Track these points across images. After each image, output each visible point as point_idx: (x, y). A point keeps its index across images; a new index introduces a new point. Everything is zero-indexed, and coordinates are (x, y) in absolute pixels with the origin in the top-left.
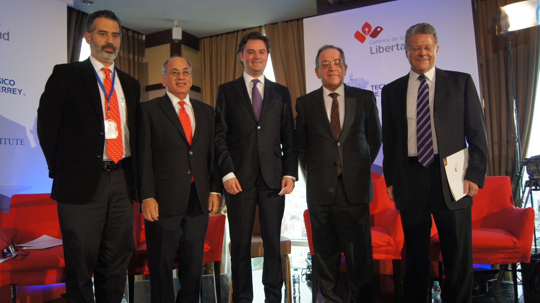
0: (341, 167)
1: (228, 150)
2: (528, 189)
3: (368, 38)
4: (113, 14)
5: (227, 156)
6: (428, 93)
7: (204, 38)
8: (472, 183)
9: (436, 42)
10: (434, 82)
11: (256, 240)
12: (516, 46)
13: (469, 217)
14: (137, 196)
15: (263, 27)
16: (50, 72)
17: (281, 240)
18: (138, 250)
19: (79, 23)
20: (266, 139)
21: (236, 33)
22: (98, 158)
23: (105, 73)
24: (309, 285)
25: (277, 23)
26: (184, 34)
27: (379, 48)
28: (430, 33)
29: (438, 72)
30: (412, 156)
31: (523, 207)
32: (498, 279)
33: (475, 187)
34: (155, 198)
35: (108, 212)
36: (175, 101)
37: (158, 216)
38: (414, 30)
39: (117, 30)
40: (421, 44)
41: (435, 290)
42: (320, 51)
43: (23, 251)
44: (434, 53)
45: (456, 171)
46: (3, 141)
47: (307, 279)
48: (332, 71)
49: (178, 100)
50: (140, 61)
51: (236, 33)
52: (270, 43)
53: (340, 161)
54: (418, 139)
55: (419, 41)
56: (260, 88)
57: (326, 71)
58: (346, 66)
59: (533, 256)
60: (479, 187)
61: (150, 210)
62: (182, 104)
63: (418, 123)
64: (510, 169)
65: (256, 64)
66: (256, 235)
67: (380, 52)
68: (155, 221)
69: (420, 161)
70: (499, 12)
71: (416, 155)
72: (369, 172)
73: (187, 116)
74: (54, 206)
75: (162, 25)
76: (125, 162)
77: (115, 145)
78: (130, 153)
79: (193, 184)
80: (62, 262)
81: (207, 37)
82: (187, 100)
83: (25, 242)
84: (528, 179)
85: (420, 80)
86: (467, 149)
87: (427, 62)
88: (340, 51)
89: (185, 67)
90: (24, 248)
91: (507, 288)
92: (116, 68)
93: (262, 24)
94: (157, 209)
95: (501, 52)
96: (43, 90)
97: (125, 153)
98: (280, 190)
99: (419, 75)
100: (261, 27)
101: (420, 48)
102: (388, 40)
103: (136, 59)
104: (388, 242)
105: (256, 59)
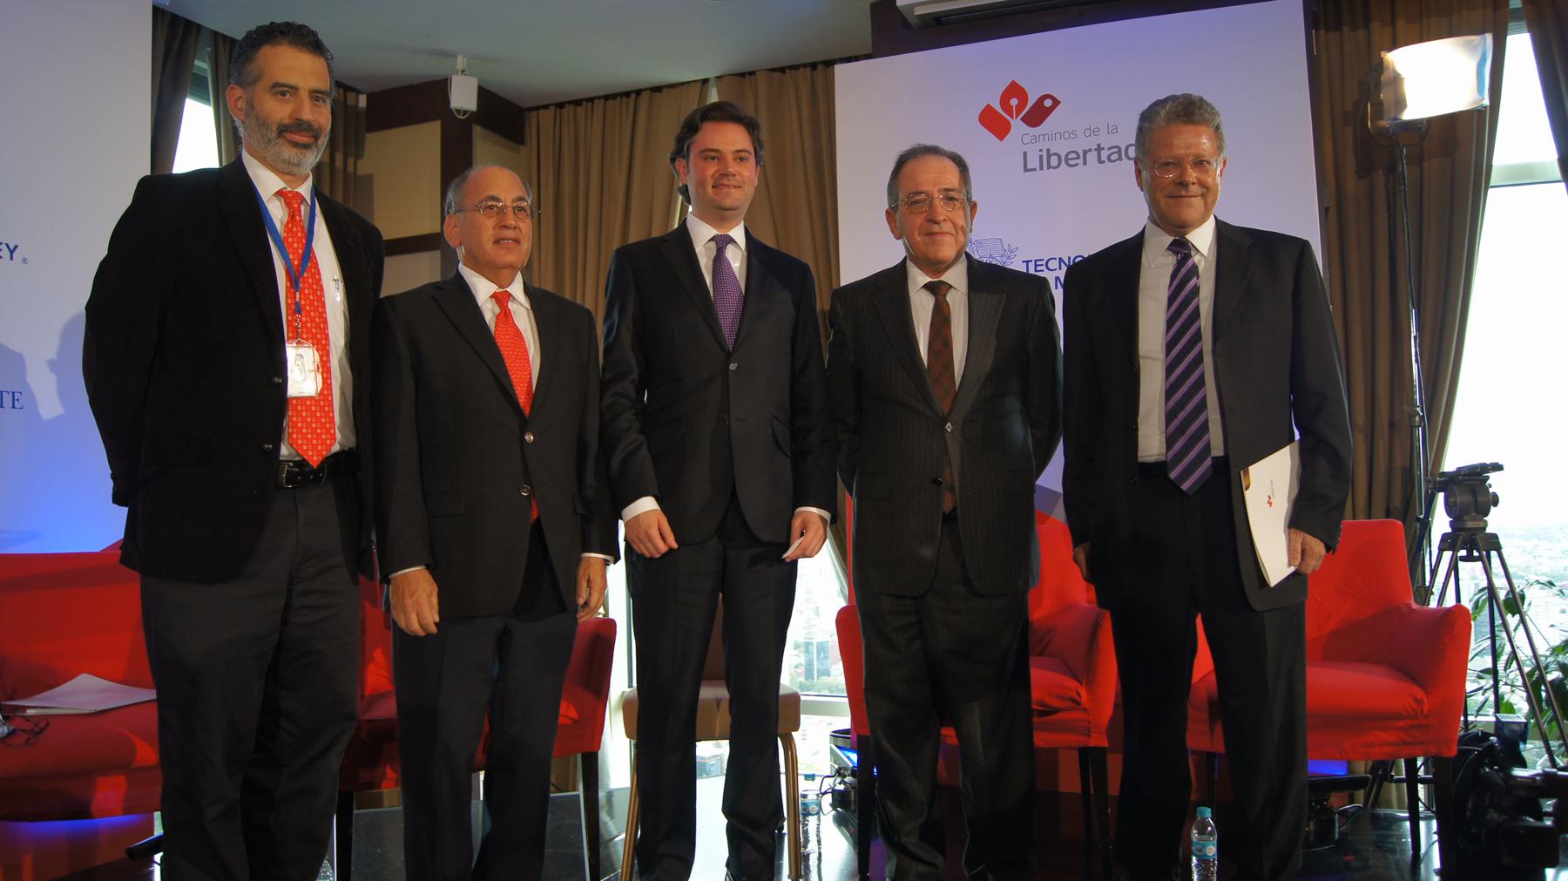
0: (952, 490)
1: (642, 432)
2: (1447, 555)
3: (1017, 125)
4: (314, 34)
5: (640, 447)
6: (1196, 291)
7: (537, 108)
8: (1309, 538)
9: (1220, 148)
10: (1213, 259)
11: (713, 693)
12: (1419, 160)
13: (1299, 629)
14: (371, 560)
15: (712, 82)
16: (125, 200)
17: (782, 692)
18: (366, 717)
19: (183, 54)
20: (754, 407)
21: (633, 96)
22: (265, 452)
23: (288, 205)
24: (840, 821)
25: (752, 73)
26: (484, 94)
27: (1049, 157)
28: (1206, 122)
29: (1224, 232)
30: (1152, 459)
31: (1433, 604)
32: (1366, 804)
33: (1318, 547)
34: (428, 567)
35: (288, 606)
36: (483, 289)
37: (437, 619)
38: (1163, 113)
39: (324, 84)
40: (1181, 152)
41: (1202, 832)
42: (902, 162)
43: (27, 718)
44: (1217, 175)
45: (1270, 503)
46: (7, 399)
47: (834, 806)
48: (937, 223)
49: (493, 288)
50: (350, 169)
51: (633, 96)
52: (764, 135)
53: (953, 473)
54: (1170, 416)
55: (1176, 142)
56: (736, 259)
57: (919, 220)
58: (974, 206)
59: (1462, 740)
60: (1328, 548)
61: (418, 603)
62: (501, 299)
63: (1169, 370)
64: (1397, 502)
65: (725, 190)
66: (713, 679)
67: (1049, 167)
68: (429, 635)
69: (1173, 475)
70: (1380, 66)
71: (1162, 458)
72: (1032, 505)
73: (518, 334)
74: (129, 591)
75: (424, 68)
76: (338, 464)
77: (313, 414)
78: (353, 440)
79: (537, 527)
80: (147, 754)
81: (546, 107)
82: (517, 289)
83: (29, 694)
84: (1449, 530)
85: (1176, 253)
86: (1295, 445)
87: (1198, 203)
88: (959, 162)
89: (520, 194)
90: (30, 712)
91: (1389, 827)
92: (316, 192)
93: (711, 74)
94: (435, 600)
95: (1380, 176)
96: (103, 252)
97: (339, 439)
98: (787, 546)
99: (1170, 239)
100: (705, 81)
101: (1178, 163)
102: (1073, 134)
103: (339, 163)
104: (1073, 701)
105: (725, 175)
